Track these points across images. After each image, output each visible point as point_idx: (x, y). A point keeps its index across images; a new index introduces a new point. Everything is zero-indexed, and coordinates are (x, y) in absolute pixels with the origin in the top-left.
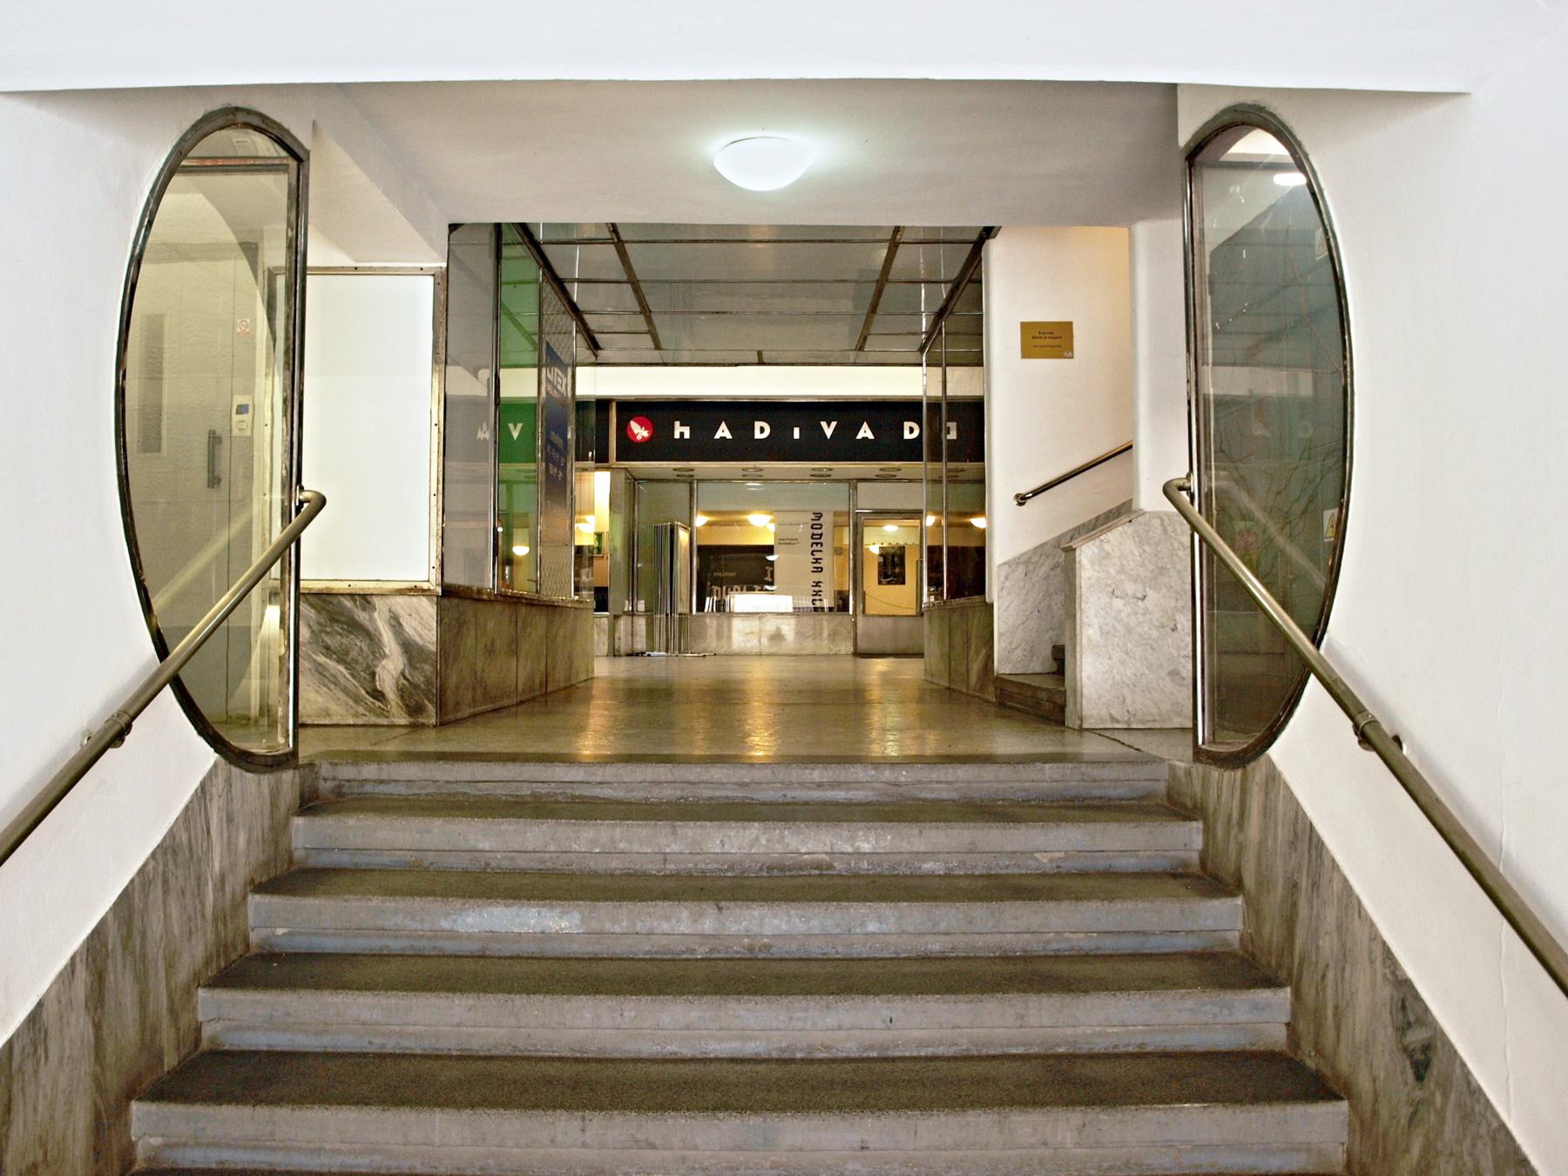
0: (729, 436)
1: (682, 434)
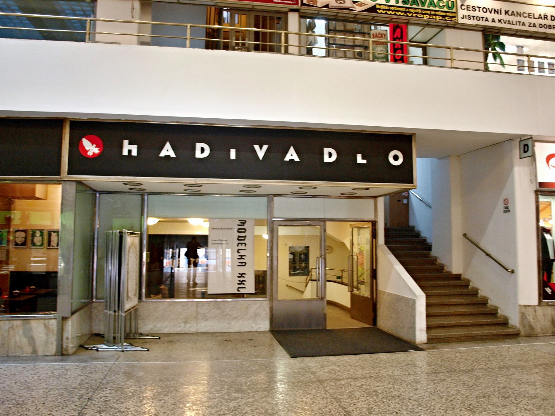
0: (297, 159)
1: (130, 151)
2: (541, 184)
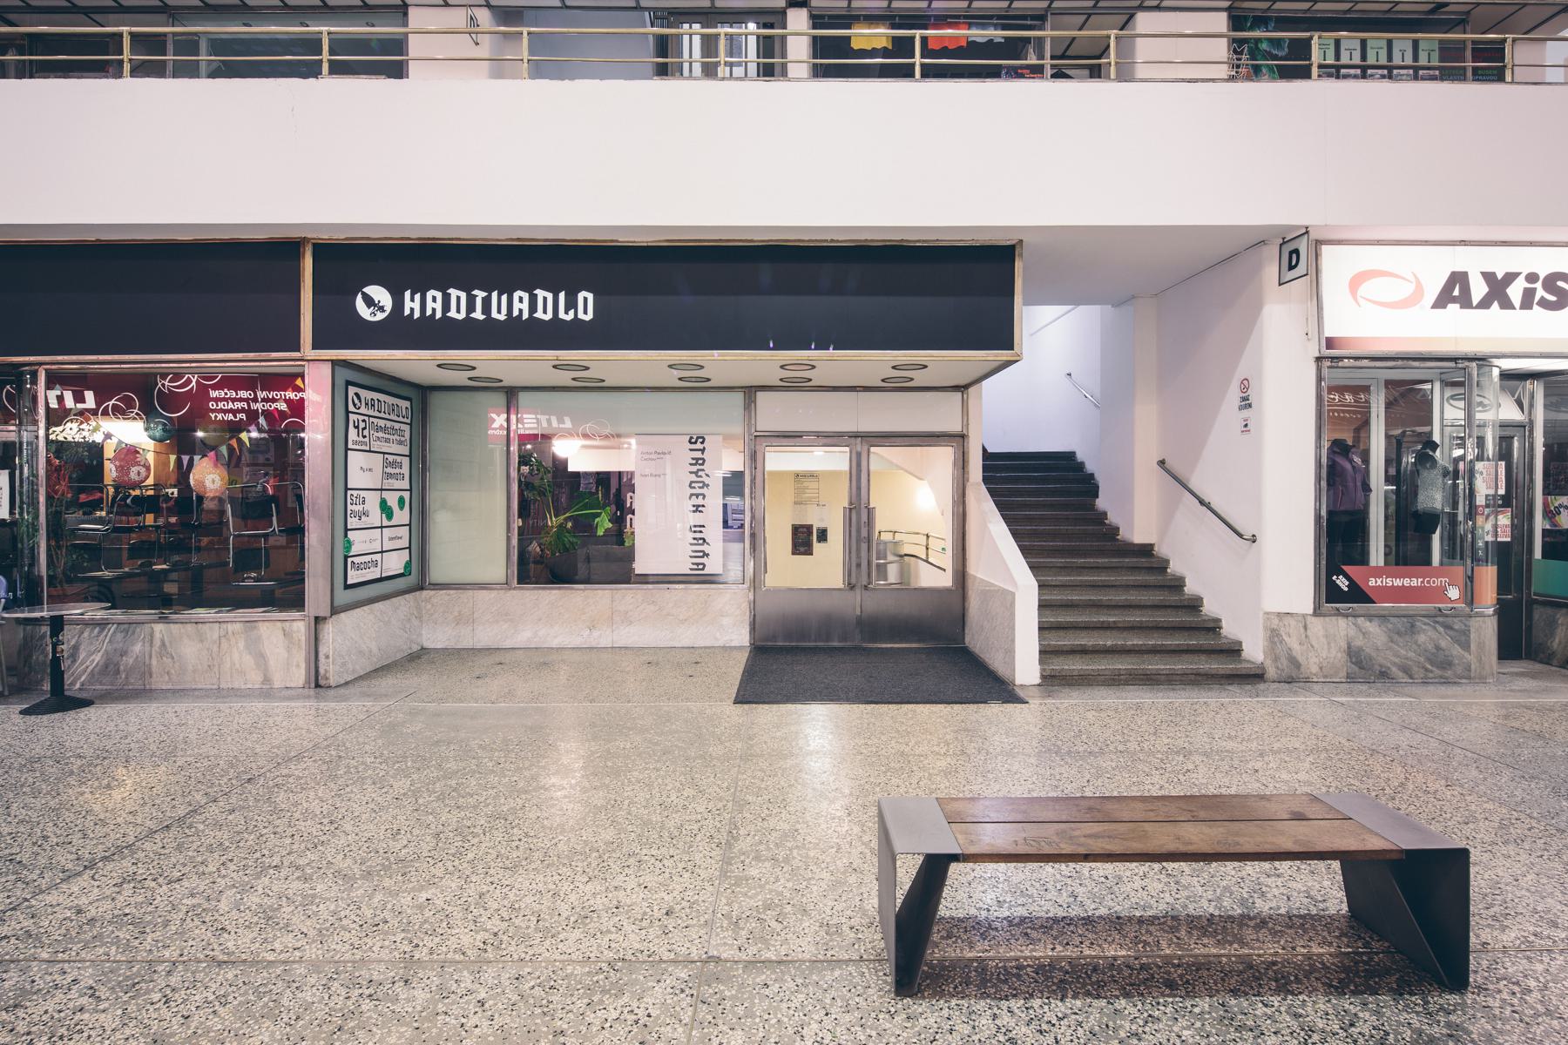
2: (1330, 342)
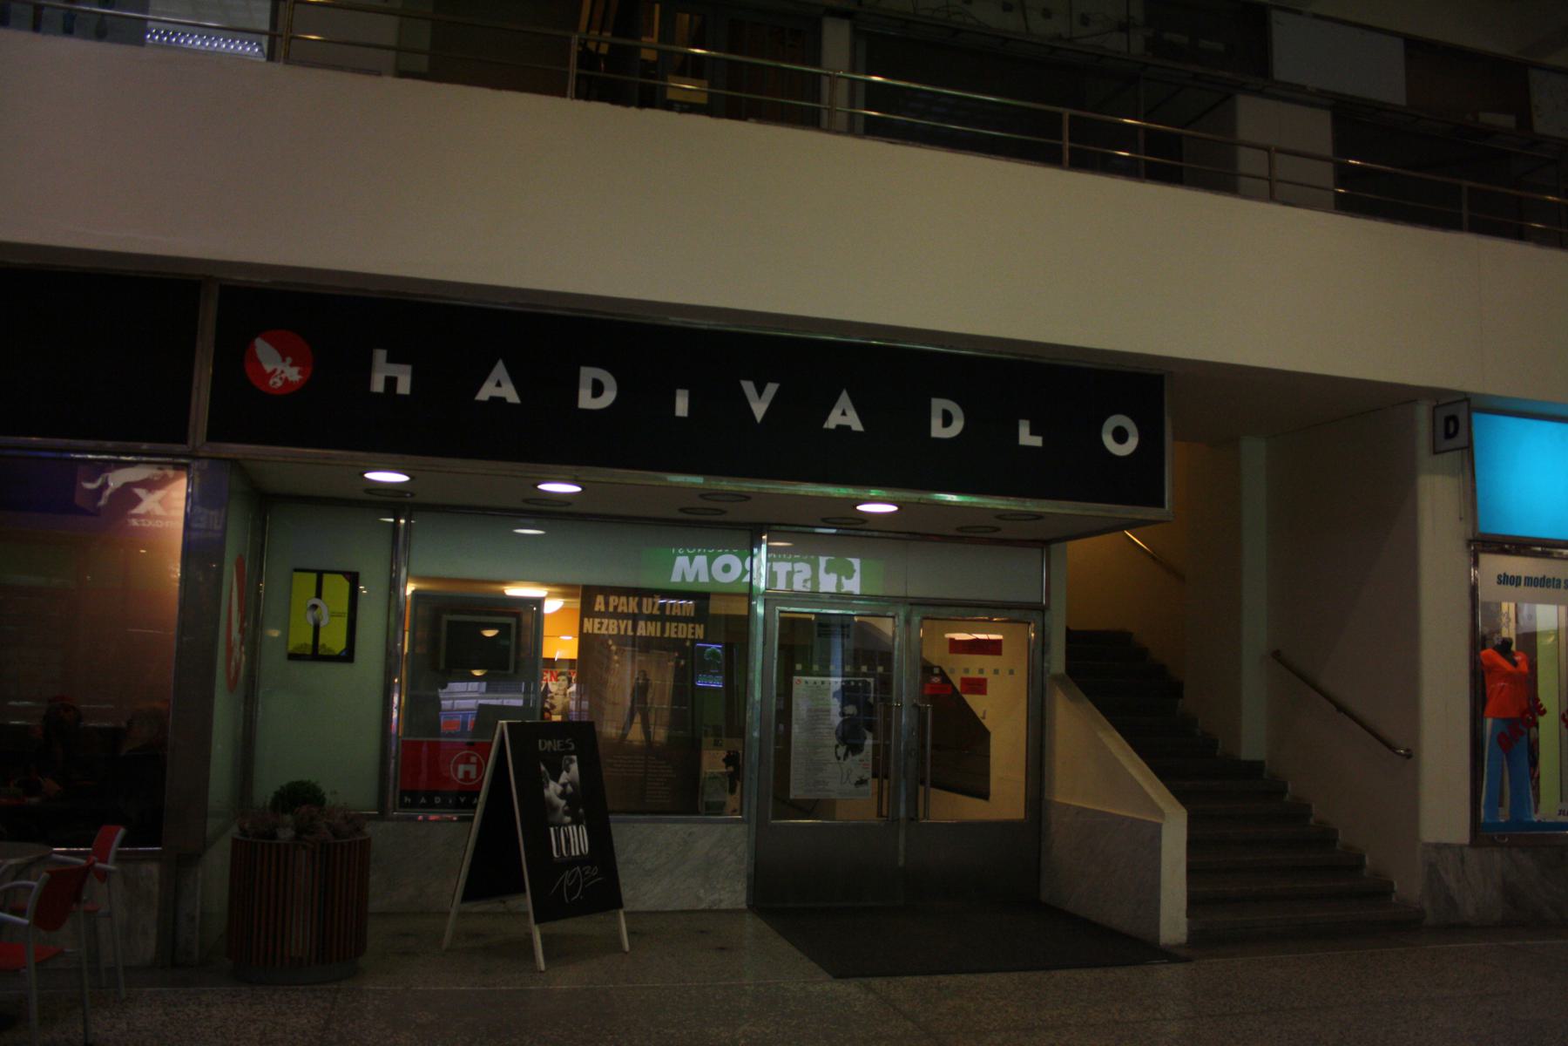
0: (857, 426)
1: (391, 382)
